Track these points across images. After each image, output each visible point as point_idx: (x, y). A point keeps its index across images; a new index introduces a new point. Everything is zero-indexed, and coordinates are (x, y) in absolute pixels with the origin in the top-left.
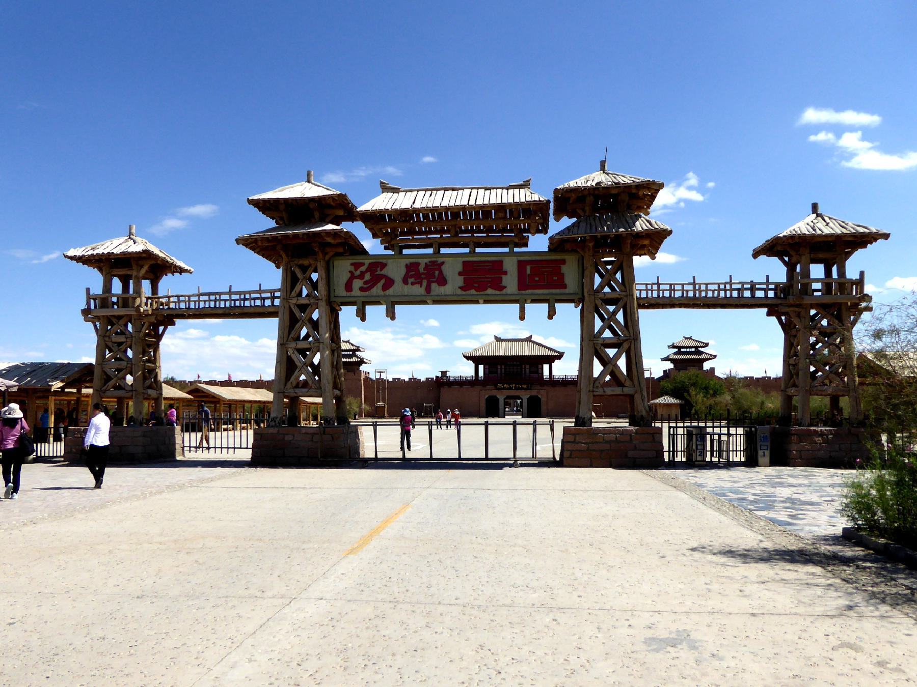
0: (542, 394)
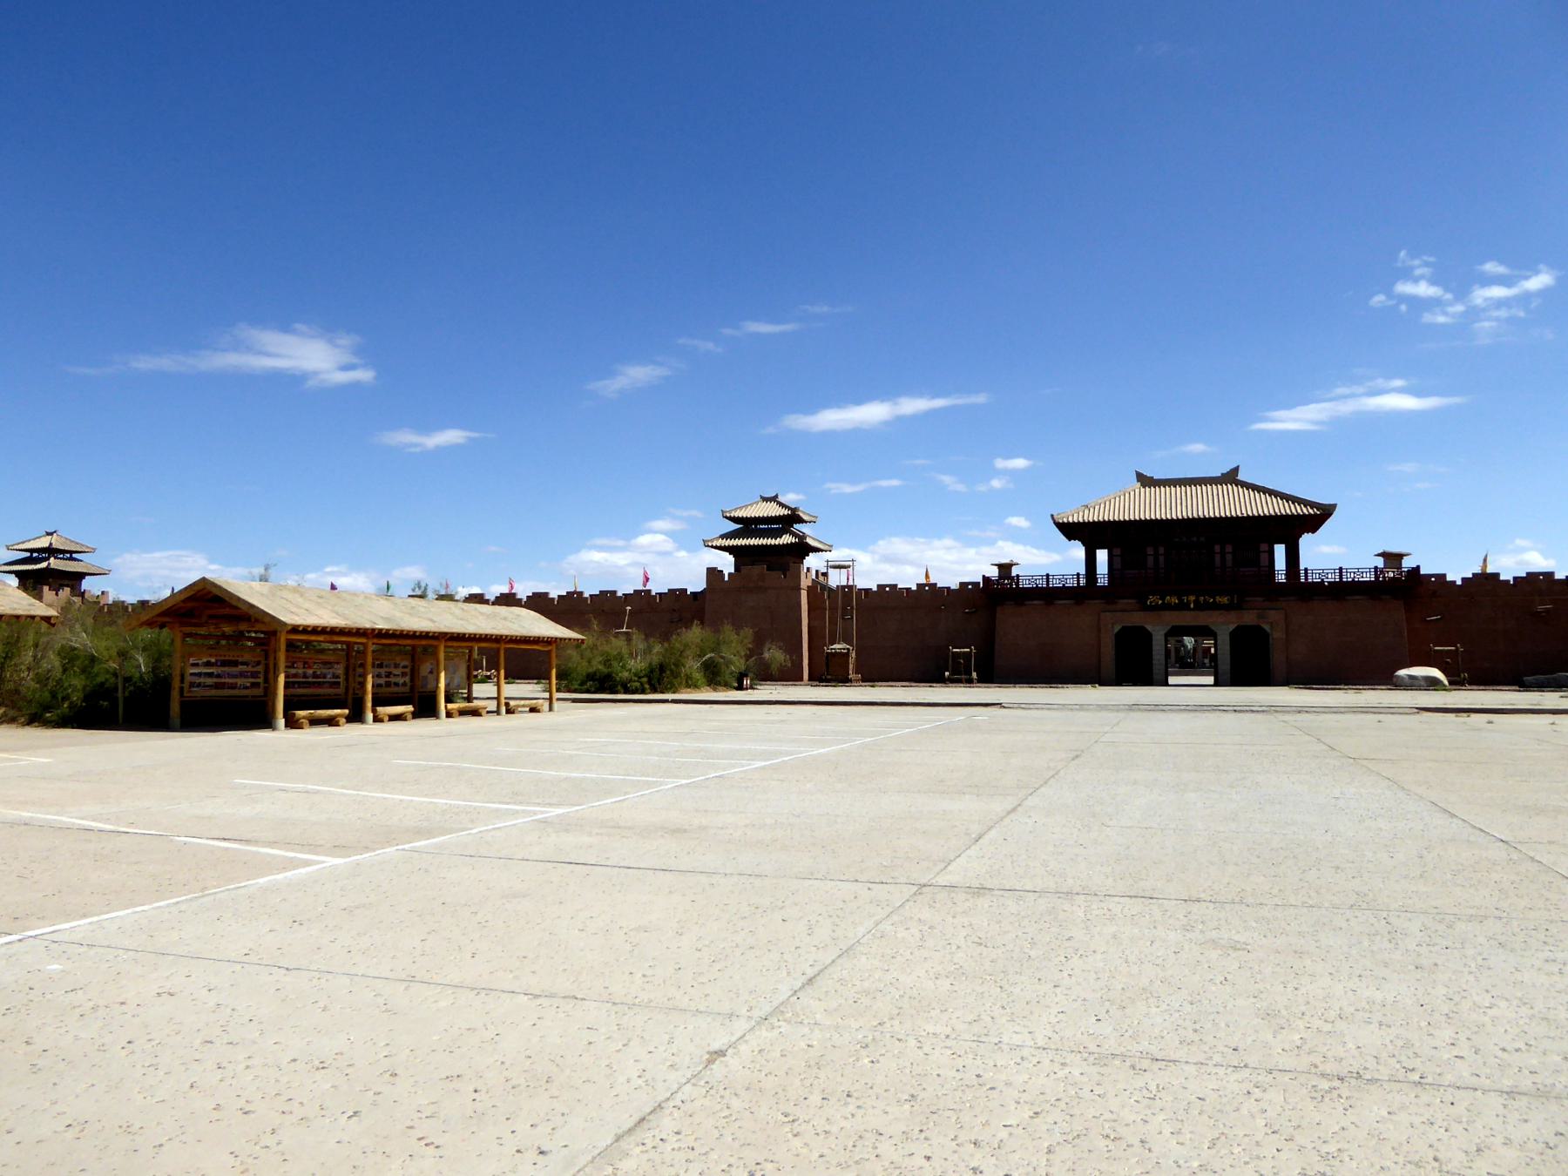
0: (1273, 622)
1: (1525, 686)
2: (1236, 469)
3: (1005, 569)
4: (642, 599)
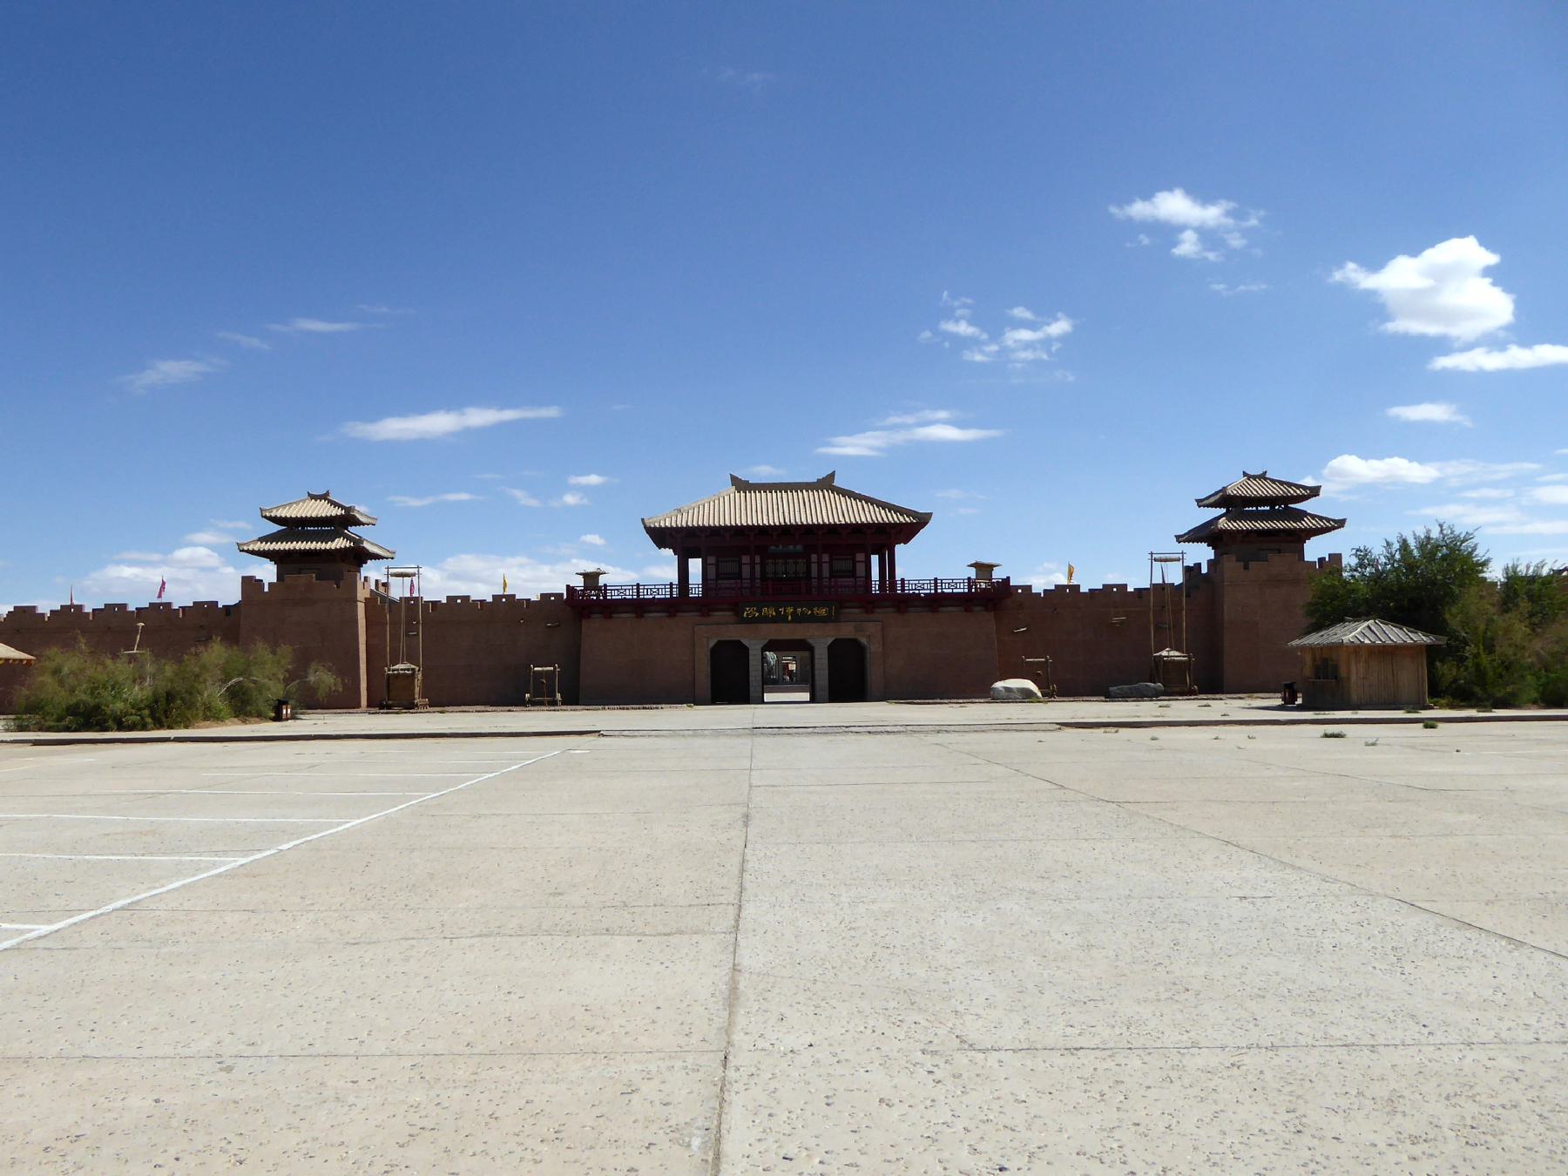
0: (869, 632)
1: (1110, 697)
2: (832, 475)
3: (591, 578)
4: (159, 614)
